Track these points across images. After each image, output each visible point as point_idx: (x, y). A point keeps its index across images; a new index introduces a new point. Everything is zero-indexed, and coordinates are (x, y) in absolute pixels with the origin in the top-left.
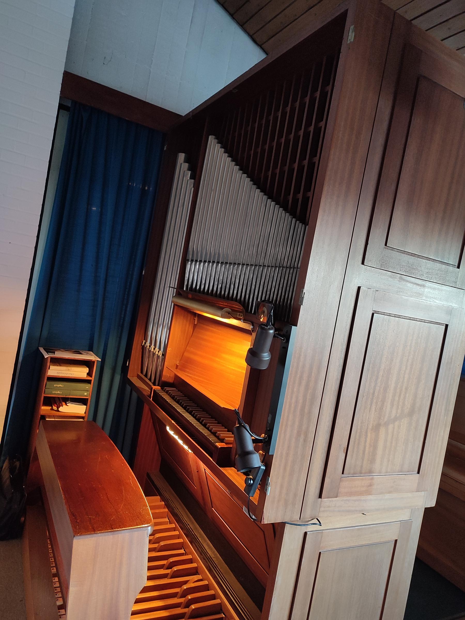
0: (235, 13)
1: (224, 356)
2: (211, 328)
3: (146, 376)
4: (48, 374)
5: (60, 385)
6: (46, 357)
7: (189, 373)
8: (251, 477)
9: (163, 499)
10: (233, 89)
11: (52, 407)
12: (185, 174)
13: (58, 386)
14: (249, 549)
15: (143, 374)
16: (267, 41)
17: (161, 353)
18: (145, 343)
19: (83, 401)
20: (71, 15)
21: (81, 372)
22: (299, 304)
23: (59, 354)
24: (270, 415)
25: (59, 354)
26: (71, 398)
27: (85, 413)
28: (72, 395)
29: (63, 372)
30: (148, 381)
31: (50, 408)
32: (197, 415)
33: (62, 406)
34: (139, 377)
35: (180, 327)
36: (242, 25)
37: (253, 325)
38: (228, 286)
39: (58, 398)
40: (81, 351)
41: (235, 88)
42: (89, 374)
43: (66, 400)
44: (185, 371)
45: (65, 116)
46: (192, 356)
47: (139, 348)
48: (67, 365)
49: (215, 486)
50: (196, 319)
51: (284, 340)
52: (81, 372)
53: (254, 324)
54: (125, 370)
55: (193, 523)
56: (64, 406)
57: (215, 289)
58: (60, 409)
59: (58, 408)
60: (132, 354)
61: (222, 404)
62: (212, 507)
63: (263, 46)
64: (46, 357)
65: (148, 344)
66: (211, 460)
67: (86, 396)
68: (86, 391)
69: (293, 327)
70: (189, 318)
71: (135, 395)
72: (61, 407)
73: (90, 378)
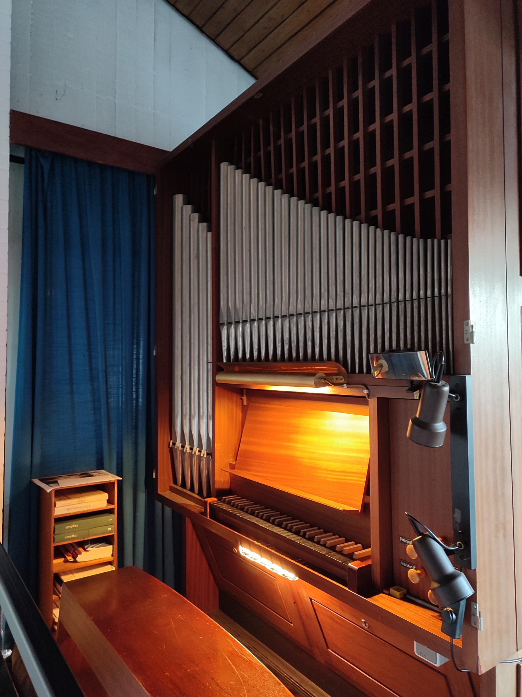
0: (204, 25)
3: (184, 485)
4: (55, 514)
5: (74, 526)
6: (48, 491)
8: (449, 609)
10: (257, 93)
11: (65, 557)
12: (191, 218)
13: (71, 527)
14: (336, 652)
15: (180, 485)
16: (247, 54)
17: (204, 452)
18: (174, 444)
19: (106, 540)
20: (8, 39)
21: (98, 501)
22: (466, 342)
23: (65, 483)
24: (456, 510)
25: (65, 483)
26: (91, 540)
27: (112, 555)
28: (93, 536)
29: (74, 506)
30: (189, 492)
31: (63, 559)
32: (292, 527)
33: (80, 553)
34: (172, 489)
35: (228, 411)
36: (214, 39)
37: (367, 389)
38: (301, 344)
39: (71, 544)
40: (89, 472)
41: (260, 91)
42: (110, 501)
43: (83, 544)
44: (249, 470)
45: (21, 169)
46: (253, 448)
48: (79, 495)
49: (333, 619)
50: (245, 398)
51: (456, 398)
52: (98, 501)
53: (368, 386)
54: (151, 485)
55: (295, 674)
56: (84, 553)
57: (279, 352)
58: (78, 559)
59: (75, 557)
60: (159, 461)
61: (341, 507)
62: (328, 648)
63: (242, 62)
64: (48, 491)
65: (178, 444)
66: (347, 589)
67: (110, 532)
68: (108, 526)
69: (467, 376)
70: (235, 400)
71: (168, 510)
72: (79, 556)
73: (111, 507)
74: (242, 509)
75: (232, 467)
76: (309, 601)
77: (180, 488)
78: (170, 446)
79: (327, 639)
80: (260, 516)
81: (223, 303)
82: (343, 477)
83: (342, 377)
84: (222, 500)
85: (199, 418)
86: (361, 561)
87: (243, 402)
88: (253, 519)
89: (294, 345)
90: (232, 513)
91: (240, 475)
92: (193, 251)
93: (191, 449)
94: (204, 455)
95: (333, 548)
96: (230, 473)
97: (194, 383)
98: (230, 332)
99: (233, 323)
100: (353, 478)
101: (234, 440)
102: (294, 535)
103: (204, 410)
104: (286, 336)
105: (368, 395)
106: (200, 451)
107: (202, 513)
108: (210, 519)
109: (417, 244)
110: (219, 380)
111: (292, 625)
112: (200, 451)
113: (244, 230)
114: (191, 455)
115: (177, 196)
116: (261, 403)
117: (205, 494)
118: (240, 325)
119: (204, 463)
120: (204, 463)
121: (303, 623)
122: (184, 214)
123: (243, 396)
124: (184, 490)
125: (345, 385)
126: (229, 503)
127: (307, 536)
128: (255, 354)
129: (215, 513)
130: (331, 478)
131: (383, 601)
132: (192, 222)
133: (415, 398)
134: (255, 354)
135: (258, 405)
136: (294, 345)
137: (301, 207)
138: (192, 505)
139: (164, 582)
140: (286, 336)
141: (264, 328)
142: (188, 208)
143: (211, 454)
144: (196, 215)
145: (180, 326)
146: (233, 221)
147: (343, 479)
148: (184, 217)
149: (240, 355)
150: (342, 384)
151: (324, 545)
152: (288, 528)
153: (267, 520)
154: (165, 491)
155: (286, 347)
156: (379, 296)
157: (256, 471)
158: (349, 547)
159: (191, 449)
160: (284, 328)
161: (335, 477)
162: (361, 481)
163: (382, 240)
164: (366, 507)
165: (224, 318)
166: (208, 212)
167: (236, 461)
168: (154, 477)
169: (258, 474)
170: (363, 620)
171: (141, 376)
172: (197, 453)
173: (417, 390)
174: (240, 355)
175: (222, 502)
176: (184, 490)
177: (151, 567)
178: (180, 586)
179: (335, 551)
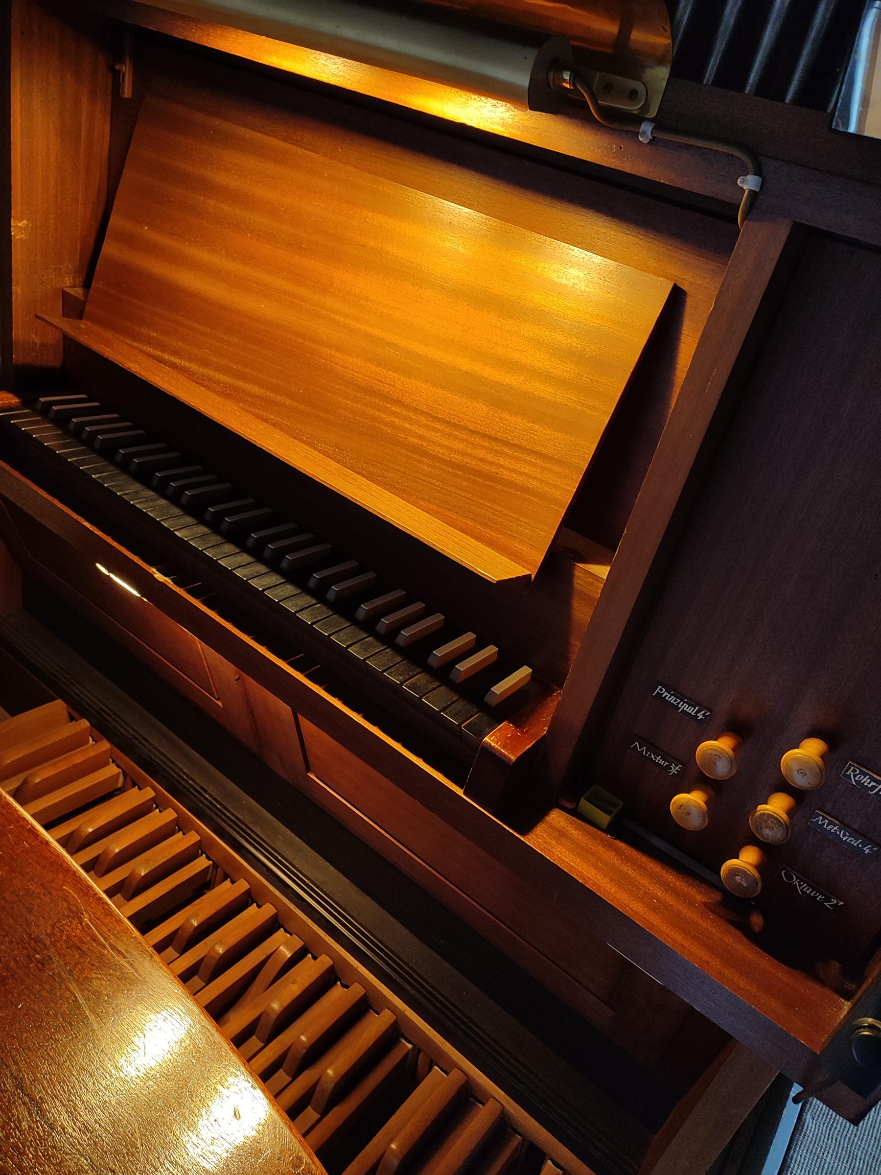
2: (249, 133)
7: (149, 341)
37: (758, 173)
44: (135, 336)
50: (126, 70)
62: (308, 770)
66: (460, 792)
74: (108, 452)
75: (74, 308)
82: (490, 457)
86: (518, 724)
87: (117, 85)
88: (147, 500)
95: (416, 654)
101: (81, 216)
102: (290, 589)
111: (219, 703)
121: (251, 713)
126: (61, 421)
131: (561, 841)
147: (492, 463)
153: (195, 510)
157: (163, 347)
164: (558, 563)
167: (87, 285)
169: (166, 356)
175: (35, 412)
179: (426, 668)
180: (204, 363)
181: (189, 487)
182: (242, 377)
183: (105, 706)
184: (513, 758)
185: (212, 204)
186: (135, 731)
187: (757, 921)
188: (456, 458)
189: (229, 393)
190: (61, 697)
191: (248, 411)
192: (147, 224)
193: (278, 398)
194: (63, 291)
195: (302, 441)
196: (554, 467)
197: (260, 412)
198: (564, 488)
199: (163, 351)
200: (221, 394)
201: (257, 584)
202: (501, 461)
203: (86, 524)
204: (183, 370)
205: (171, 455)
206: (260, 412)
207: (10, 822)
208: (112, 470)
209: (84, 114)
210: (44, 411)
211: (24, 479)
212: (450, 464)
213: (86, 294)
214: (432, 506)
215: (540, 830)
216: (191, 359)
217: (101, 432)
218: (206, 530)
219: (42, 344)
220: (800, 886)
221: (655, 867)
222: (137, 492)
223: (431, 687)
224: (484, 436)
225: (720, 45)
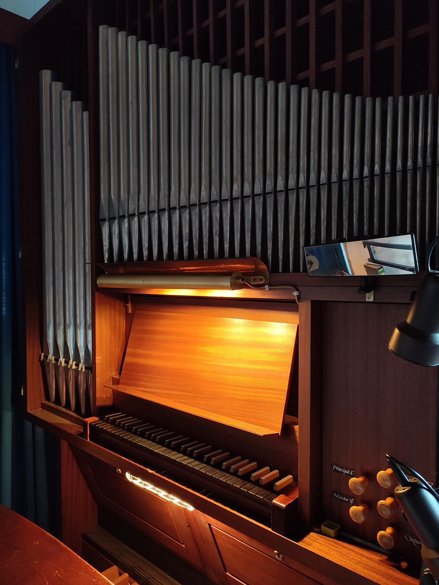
1: (210, 349)
2: (167, 314)
3: (58, 401)
7: (142, 386)
9: (123, 568)
14: (234, 574)
15: (53, 402)
18: (46, 357)
30: (64, 410)
34: (44, 407)
37: (297, 290)
38: (206, 240)
44: (136, 386)
47: (37, 365)
50: (129, 305)
54: (19, 403)
57: (176, 249)
61: (261, 431)
62: (226, 571)
65: (51, 357)
66: (270, 530)
71: (40, 431)
74: (129, 430)
76: (208, 526)
77: (53, 405)
78: (42, 360)
79: (226, 563)
80: (152, 438)
81: (104, 195)
82: (256, 395)
83: (262, 277)
84: (105, 419)
85: (79, 333)
86: (287, 495)
87: (127, 310)
88: (144, 442)
89: (195, 241)
90: (118, 436)
91: (127, 392)
92: (66, 136)
93: (67, 362)
94: (82, 369)
95: (246, 477)
96: (113, 390)
97: (69, 289)
98: (113, 229)
99: (117, 218)
100: (269, 395)
101: (118, 352)
102: (197, 463)
103: (81, 319)
104: (186, 231)
105: (299, 297)
106: (77, 365)
107: (81, 435)
108: (91, 442)
109: (372, 106)
110: (100, 284)
111: (183, 546)
112: (77, 365)
113: (130, 106)
114: (67, 369)
115: (44, 71)
116: (150, 311)
117: (83, 410)
118: (126, 220)
119: (81, 378)
120: (81, 378)
121: (197, 546)
122: (52, 90)
123: (128, 303)
124: (59, 408)
125: (266, 286)
126: (113, 423)
127: (212, 463)
128: (145, 253)
129: (97, 435)
130: (239, 395)
131: (316, 544)
132: (63, 101)
133: (367, 300)
134: (145, 253)
135: (146, 312)
136: (195, 241)
137: (207, 70)
138: (68, 425)
139: (36, 523)
140: (186, 231)
141: (157, 222)
142: (58, 86)
143: (91, 368)
144: (68, 94)
145: (50, 225)
146: (115, 95)
147: (257, 397)
148: (54, 95)
149: (126, 256)
150: (263, 285)
151: (235, 474)
152: (188, 452)
153: (161, 443)
154: (35, 409)
155: (186, 245)
156: (313, 176)
157: (146, 387)
158: (266, 474)
159: (67, 362)
160: (183, 222)
161: (245, 393)
162: (280, 399)
163: (322, 102)
164: (287, 428)
165: (105, 213)
166: (84, 87)
167: (120, 374)
168: (22, 395)
169: (147, 390)
170: (276, 552)
171: (4, 282)
172: (74, 367)
173: (369, 292)
174: (126, 256)
175: (104, 421)
176: (59, 408)
177: (20, 505)
178: (56, 529)
179: (250, 481)
180: (159, 388)
181: (158, 435)
182: (172, 390)
183: (135, 564)
184: (284, 506)
185: (158, 337)
186: (149, 575)
187: (404, 565)
188: (246, 398)
189: (169, 397)
190: (115, 565)
191: (176, 401)
192: (138, 348)
193: (186, 394)
194: (113, 377)
195: (195, 407)
196: (277, 392)
197: (180, 400)
198: (282, 399)
199: (146, 388)
200: (166, 397)
201: (185, 463)
202: (260, 395)
203: (123, 458)
204: (153, 393)
205: (152, 426)
206: (180, 400)
207: (100, 581)
208: (132, 435)
209: (117, 321)
210: (107, 421)
211: (101, 447)
212: (244, 400)
213: (120, 377)
214: (241, 418)
215: (306, 539)
216: (155, 388)
217: (127, 423)
218: (165, 448)
219: (106, 397)
220: (414, 541)
221: (357, 549)
222: (140, 440)
223: (252, 487)
224: (253, 388)
225: (281, 263)
